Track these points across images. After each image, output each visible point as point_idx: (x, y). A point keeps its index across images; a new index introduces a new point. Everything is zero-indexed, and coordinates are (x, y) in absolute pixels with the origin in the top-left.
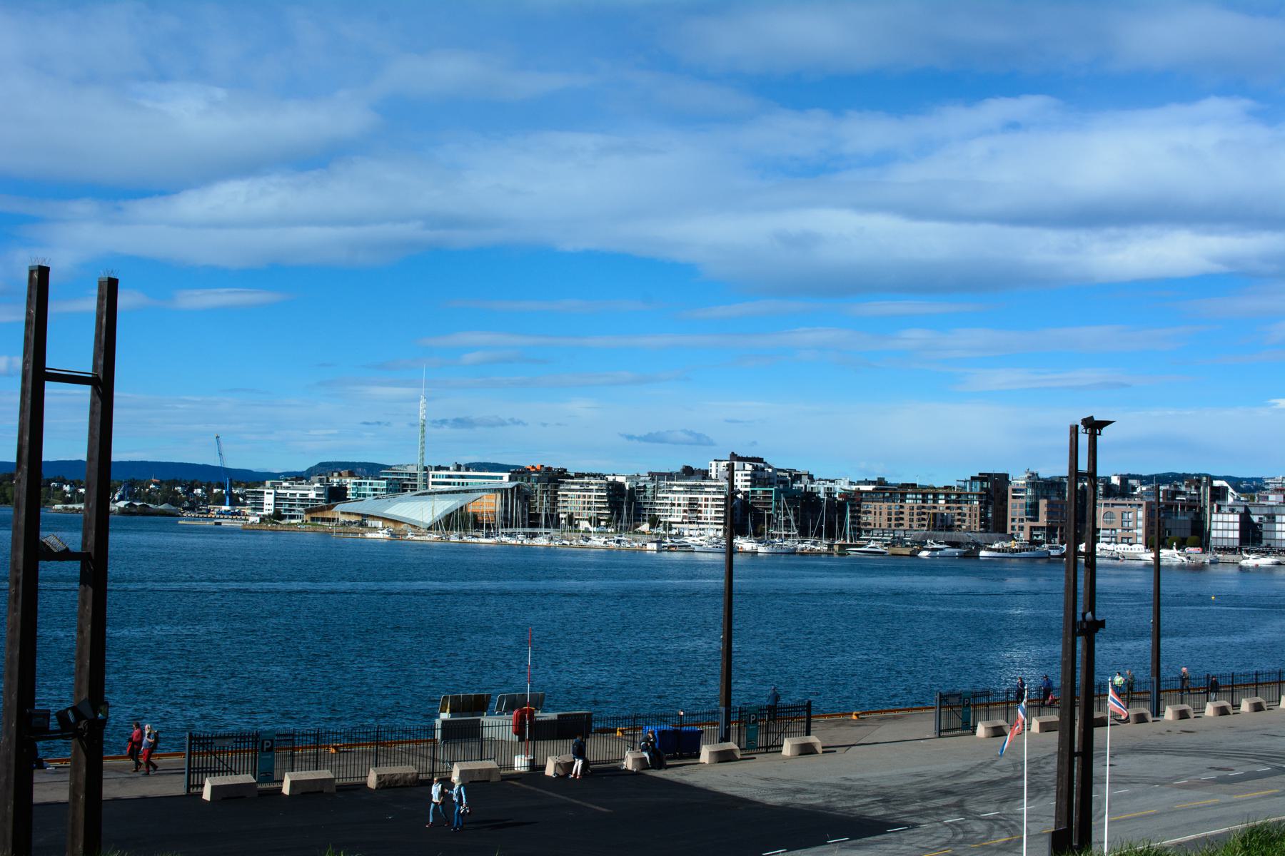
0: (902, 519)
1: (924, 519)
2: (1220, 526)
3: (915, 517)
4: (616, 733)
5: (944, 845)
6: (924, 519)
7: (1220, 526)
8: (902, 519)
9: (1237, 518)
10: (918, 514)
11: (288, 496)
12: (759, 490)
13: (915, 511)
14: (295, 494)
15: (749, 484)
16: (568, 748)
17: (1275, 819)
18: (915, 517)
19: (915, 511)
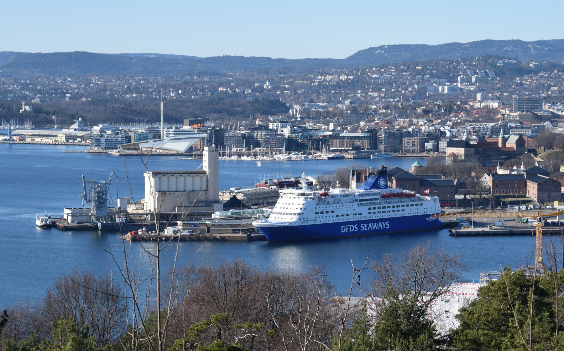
0: (344, 145)
1: (351, 145)
2: (441, 145)
3: (348, 144)
4: (103, 225)
5: (395, 339)
6: (351, 145)
7: (441, 145)
8: (344, 145)
9: (446, 143)
10: (349, 143)
11: (110, 140)
12: (294, 135)
13: (348, 142)
14: (113, 140)
15: (290, 133)
16: (500, 228)
17: (169, 213)
18: (348, 144)
19: (348, 142)
